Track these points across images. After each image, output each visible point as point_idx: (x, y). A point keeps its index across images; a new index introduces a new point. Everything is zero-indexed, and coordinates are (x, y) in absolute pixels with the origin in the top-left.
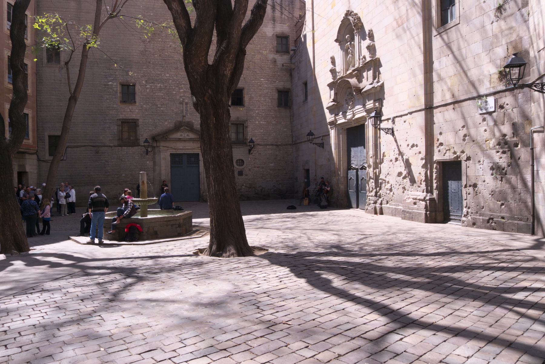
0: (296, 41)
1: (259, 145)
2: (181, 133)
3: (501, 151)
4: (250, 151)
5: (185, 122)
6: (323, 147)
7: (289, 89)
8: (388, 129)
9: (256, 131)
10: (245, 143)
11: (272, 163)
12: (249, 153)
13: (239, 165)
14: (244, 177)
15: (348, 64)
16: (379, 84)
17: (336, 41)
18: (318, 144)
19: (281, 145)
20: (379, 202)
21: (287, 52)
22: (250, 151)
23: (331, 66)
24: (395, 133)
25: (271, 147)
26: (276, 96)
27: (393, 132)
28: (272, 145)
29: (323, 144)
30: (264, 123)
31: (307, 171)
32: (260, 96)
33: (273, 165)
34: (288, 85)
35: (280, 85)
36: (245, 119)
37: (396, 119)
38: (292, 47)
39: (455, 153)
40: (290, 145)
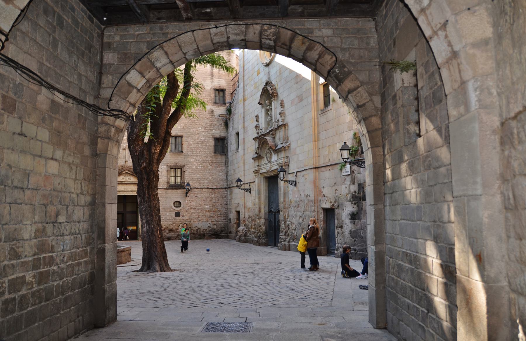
0: (232, 94)
1: (195, 188)
2: (123, 177)
3: (353, 202)
4: (187, 193)
5: (127, 167)
6: (250, 192)
7: (225, 137)
8: (248, 189)
9: (193, 175)
10: (183, 186)
11: (207, 205)
12: (186, 196)
13: (177, 207)
14: (180, 218)
15: (269, 123)
16: (287, 144)
17: (259, 103)
18: (290, 181)
19: (217, 189)
20: (288, 240)
21: (224, 103)
22: (187, 193)
23: (255, 123)
24: (297, 184)
25: (206, 190)
26: (212, 143)
27: (296, 183)
28: (208, 188)
29: (250, 189)
30: (200, 168)
31: (238, 213)
32: (198, 143)
33: (208, 207)
34: (223, 134)
35: (218, 133)
36: (183, 164)
37: (298, 173)
38: (228, 100)
39: (331, 202)
40: (225, 188)
